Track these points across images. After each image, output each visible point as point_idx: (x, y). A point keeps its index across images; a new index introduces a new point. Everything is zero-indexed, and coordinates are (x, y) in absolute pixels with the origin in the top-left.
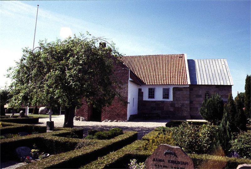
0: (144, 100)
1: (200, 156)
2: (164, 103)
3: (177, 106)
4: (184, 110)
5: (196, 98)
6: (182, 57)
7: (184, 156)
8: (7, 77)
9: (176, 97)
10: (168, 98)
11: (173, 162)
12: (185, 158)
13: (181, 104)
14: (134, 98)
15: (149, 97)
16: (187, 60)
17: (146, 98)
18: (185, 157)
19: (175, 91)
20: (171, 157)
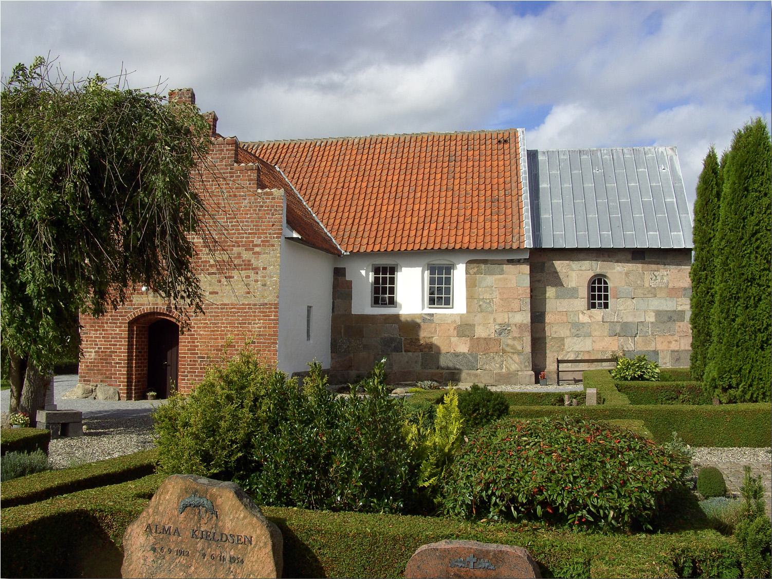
0: (353, 313)
1: (227, 508)
2: (431, 321)
3: (484, 335)
4: (508, 349)
5: (558, 301)
6: (506, 141)
7: (242, 516)
8: (97, 74)
9: (479, 300)
10: (448, 302)
11: (206, 536)
12: (246, 521)
13: (497, 327)
14: (309, 308)
15: (376, 302)
16: (537, 151)
17: (362, 304)
18: (245, 518)
19: (475, 274)
20: (202, 522)
